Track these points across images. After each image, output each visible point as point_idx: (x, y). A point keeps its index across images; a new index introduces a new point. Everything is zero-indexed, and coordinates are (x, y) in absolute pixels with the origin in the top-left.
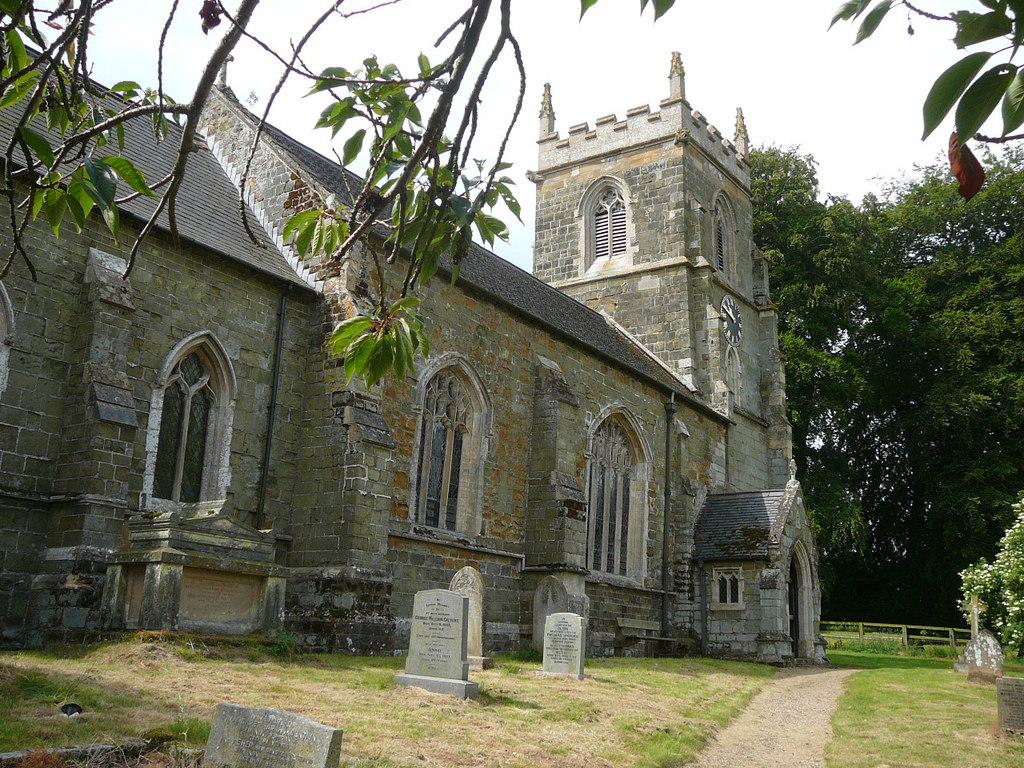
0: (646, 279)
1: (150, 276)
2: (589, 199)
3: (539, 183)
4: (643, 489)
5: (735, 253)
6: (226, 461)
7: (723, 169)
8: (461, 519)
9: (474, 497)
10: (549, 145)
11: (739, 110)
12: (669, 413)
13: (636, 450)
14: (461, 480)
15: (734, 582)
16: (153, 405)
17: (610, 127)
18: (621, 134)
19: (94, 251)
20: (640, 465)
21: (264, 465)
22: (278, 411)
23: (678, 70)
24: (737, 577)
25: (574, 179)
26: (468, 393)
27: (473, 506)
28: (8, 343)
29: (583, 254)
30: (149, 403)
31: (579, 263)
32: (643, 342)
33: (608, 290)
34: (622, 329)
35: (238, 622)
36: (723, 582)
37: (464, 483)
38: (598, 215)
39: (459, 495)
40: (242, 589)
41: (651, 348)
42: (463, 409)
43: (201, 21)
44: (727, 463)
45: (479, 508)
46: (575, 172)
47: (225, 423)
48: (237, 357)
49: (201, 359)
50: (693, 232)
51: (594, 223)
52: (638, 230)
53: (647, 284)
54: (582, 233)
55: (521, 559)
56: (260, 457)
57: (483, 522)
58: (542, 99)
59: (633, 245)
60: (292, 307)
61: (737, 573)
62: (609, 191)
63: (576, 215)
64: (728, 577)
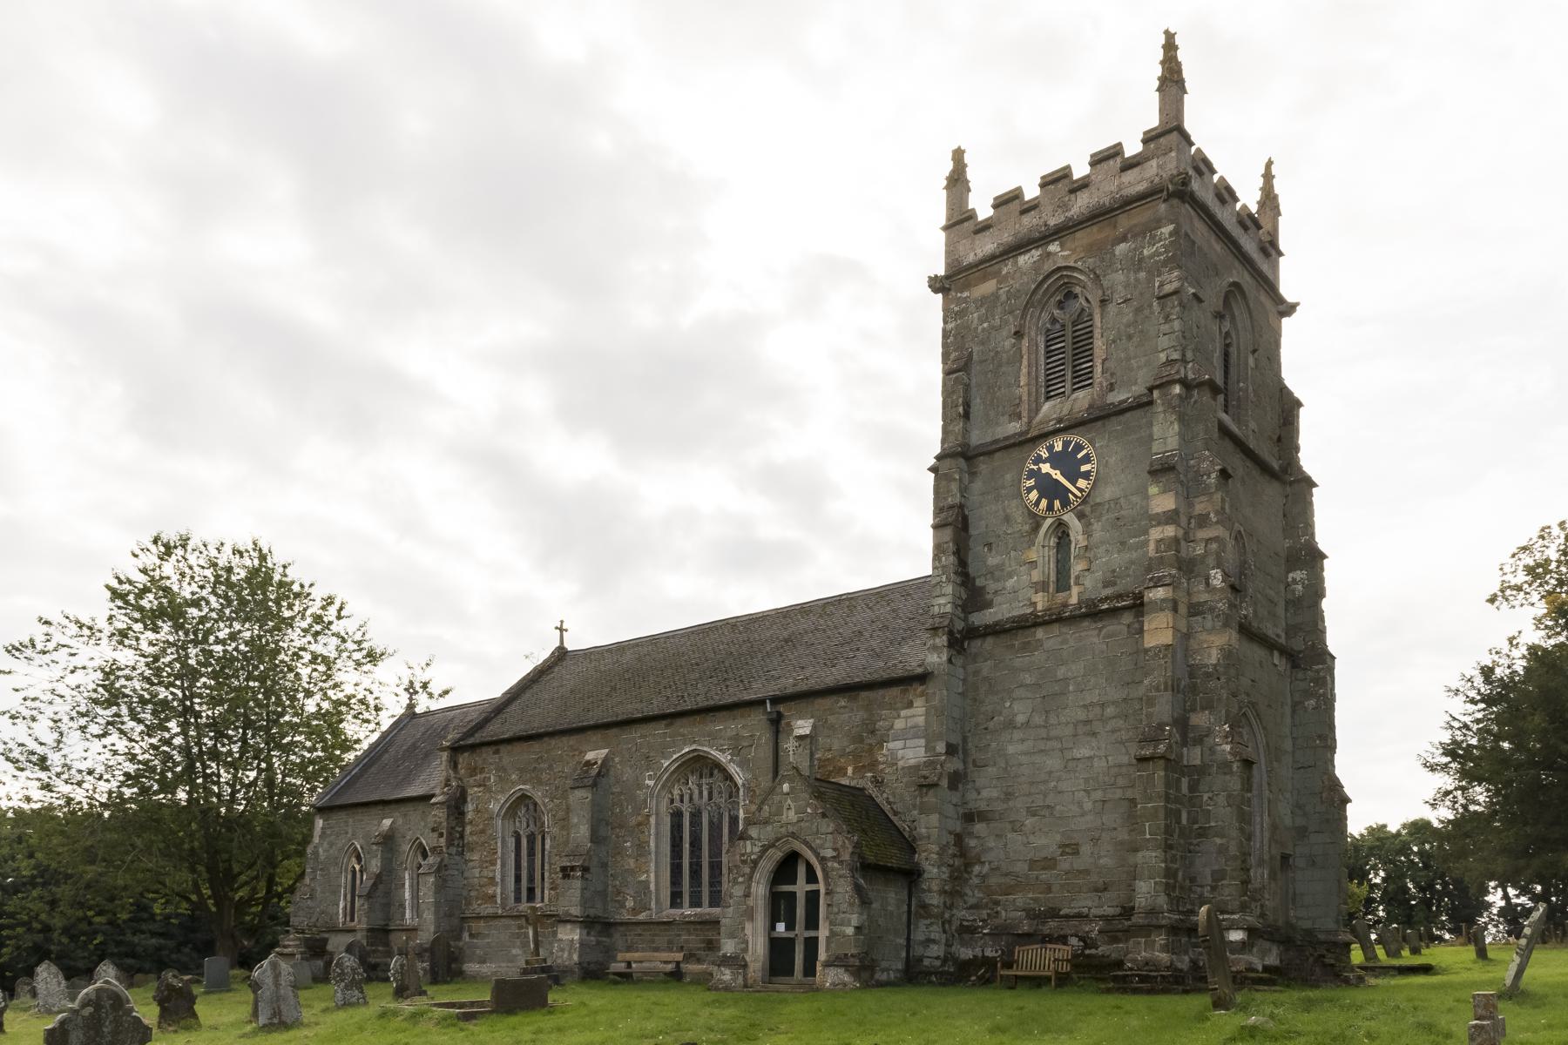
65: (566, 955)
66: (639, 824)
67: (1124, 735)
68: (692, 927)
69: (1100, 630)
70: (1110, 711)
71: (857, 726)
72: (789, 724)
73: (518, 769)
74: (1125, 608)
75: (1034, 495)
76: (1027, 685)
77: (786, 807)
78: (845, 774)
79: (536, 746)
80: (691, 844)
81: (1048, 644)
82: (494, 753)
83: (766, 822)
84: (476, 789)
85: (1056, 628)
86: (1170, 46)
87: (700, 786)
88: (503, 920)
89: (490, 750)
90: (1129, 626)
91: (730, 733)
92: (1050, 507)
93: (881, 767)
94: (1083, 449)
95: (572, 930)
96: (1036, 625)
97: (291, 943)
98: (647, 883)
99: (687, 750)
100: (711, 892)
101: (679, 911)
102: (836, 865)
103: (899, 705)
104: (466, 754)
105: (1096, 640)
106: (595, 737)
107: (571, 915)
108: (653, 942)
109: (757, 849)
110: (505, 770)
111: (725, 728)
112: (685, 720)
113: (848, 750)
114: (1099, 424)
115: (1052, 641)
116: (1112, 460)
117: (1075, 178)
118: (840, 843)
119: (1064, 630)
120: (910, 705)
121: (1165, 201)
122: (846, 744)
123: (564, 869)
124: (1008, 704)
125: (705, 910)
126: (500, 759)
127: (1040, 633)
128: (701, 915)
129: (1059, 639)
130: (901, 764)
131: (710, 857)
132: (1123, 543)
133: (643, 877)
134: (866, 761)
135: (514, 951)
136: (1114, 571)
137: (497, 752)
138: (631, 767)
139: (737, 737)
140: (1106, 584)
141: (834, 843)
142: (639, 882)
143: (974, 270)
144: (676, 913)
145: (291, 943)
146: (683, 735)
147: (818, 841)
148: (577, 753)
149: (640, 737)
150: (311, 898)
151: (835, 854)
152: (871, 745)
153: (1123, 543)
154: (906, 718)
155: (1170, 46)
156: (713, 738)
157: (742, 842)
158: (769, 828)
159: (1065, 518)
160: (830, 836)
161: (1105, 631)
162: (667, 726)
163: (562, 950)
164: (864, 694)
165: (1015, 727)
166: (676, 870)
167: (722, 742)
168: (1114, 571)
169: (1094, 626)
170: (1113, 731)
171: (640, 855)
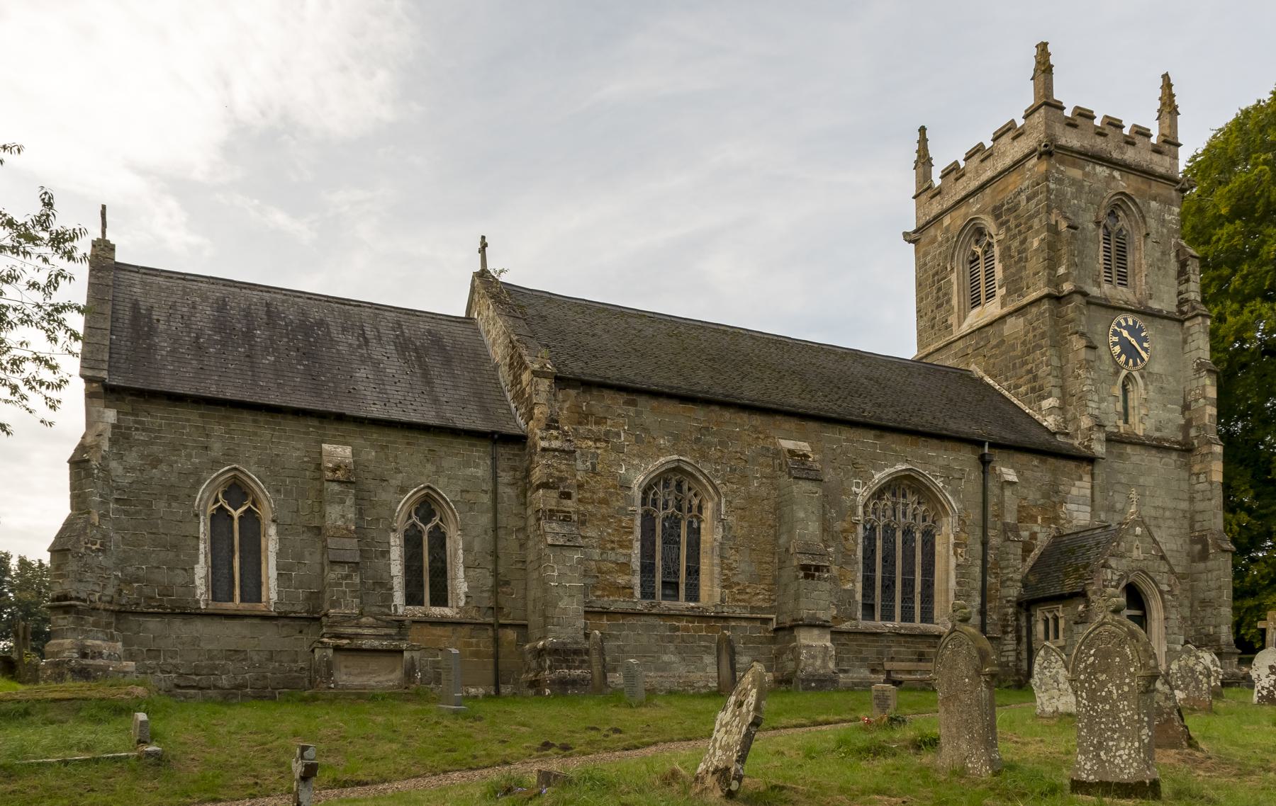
0: (1011, 321)
1: (373, 454)
2: (960, 247)
3: (914, 242)
4: (948, 542)
5: (1143, 262)
6: (461, 573)
7: (1120, 165)
8: (704, 591)
9: (712, 573)
10: (924, 197)
11: (1166, 77)
12: (985, 462)
13: (939, 506)
14: (702, 561)
15: (1056, 619)
16: (392, 544)
17: (976, 159)
18: (989, 163)
19: (325, 446)
20: (944, 519)
21: (495, 573)
22: (501, 533)
23: (1044, 68)
24: (1057, 614)
25: (947, 229)
26: (697, 488)
27: (712, 580)
28: (274, 521)
29: (956, 309)
30: (389, 543)
31: (953, 320)
32: (1009, 390)
33: (977, 343)
34: (991, 382)
35: (387, 681)
36: (1046, 621)
37: (705, 565)
38: (972, 262)
39: (701, 573)
40: (386, 661)
41: (1016, 395)
42: (695, 502)
43: (1050, 49)
44: (1093, 501)
45: (717, 581)
46: (947, 221)
47: (455, 545)
48: (458, 498)
49: (427, 507)
50: (1059, 258)
51: (968, 271)
52: (1005, 269)
53: (1014, 326)
54: (955, 287)
55: (772, 619)
56: (491, 567)
57: (722, 593)
58: (916, 146)
59: (1000, 287)
60: (503, 451)
61: (1058, 610)
62: (980, 232)
63: (949, 269)
64: (1050, 616)
65: (819, 662)
66: (845, 531)
67: (1174, 532)
68: (902, 639)
69: (1162, 458)
70: (1168, 514)
71: (1046, 485)
72: (994, 468)
73: (671, 434)
74: (1176, 450)
75: (1117, 349)
76: (1122, 483)
77: (1135, 545)
78: (1036, 522)
79: (700, 413)
80: (884, 559)
81: (1135, 459)
82: (626, 403)
83: (1122, 556)
84: (590, 443)
85: (1138, 448)
86: (1167, 83)
87: (895, 504)
88: (643, 618)
89: (621, 398)
90: (1175, 461)
91: (941, 462)
92: (1127, 363)
93: (1062, 522)
94: (1115, 330)
95: (820, 637)
96: (1131, 443)
97: (366, 631)
98: (851, 593)
99: (688, 460)
100: (922, 608)
101: (889, 624)
102: (1170, 597)
103: (1074, 476)
104: (573, 392)
105: (1159, 465)
106: (791, 424)
107: (818, 619)
108: (861, 653)
109: (1116, 578)
110: (646, 430)
111: (937, 456)
112: (895, 437)
113: (1039, 503)
114: (1150, 318)
115: (1136, 457)
116: (1158, 347)
117: (1018, 126)
118: (1173, 581)
119: (1143, 452)
120: (1080, 479)
121: (1176, 190)
122: (1038, 497)
123: (805, 568)
124: (1111, 494)
125: (918, 625)
126: (638, 414)
127: (1129, 449)
128: (912, 629)
129: (1140, 457)
130: (1074, 522)
131: (903, 574)
132: (1165, 406)
133: (849, 586)
134: (1051, 515)
135: (666, 658)
136: (1160, 422)
137: (632, 403)
138: (834, 469)
139: (947, 468)
140: (1158, 430)
141: (1169, 580)
142: (844, 590)
143: (1069, 154)
144: (417, 611)
145: (366, 631)
146: (896, 451)
147: (1158, 578)
148: (761, 436)
149: (847, 440)
150: (103, 549)
151: (1169, 589)
152: (1054, 502)
153: (1165, 406)
154: (1079, 488)
155: (1167, 83)
156: (926, 461)
157: (1104, 570)
158: (1124, 561)
159: (1134, 373)
160: (1166, 575)
161: (1163, 460)
162: (877, 437)
163: (814, 657)
164: (1051, 460)
165: (1115, 511)
166: (868, 583)
167: (934, 468)
168: (1160, 422)
169: (1158, 455)
170: (1169, 528)
171: (845, 563)
